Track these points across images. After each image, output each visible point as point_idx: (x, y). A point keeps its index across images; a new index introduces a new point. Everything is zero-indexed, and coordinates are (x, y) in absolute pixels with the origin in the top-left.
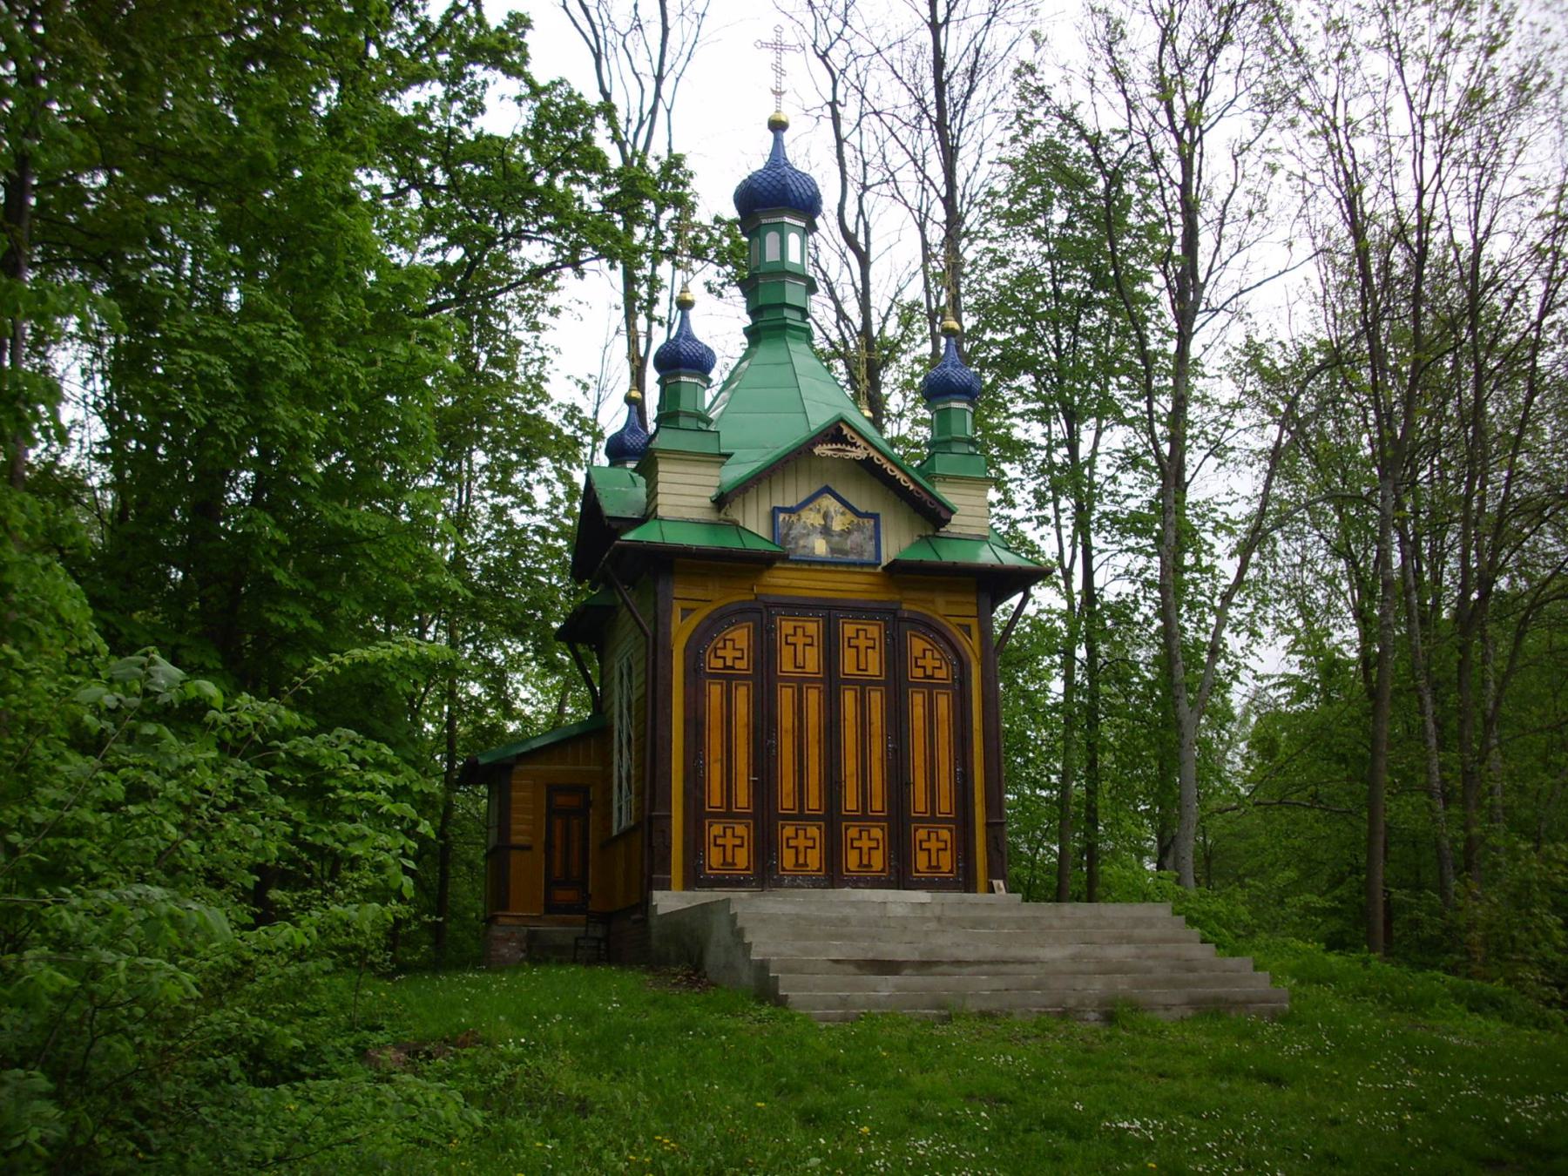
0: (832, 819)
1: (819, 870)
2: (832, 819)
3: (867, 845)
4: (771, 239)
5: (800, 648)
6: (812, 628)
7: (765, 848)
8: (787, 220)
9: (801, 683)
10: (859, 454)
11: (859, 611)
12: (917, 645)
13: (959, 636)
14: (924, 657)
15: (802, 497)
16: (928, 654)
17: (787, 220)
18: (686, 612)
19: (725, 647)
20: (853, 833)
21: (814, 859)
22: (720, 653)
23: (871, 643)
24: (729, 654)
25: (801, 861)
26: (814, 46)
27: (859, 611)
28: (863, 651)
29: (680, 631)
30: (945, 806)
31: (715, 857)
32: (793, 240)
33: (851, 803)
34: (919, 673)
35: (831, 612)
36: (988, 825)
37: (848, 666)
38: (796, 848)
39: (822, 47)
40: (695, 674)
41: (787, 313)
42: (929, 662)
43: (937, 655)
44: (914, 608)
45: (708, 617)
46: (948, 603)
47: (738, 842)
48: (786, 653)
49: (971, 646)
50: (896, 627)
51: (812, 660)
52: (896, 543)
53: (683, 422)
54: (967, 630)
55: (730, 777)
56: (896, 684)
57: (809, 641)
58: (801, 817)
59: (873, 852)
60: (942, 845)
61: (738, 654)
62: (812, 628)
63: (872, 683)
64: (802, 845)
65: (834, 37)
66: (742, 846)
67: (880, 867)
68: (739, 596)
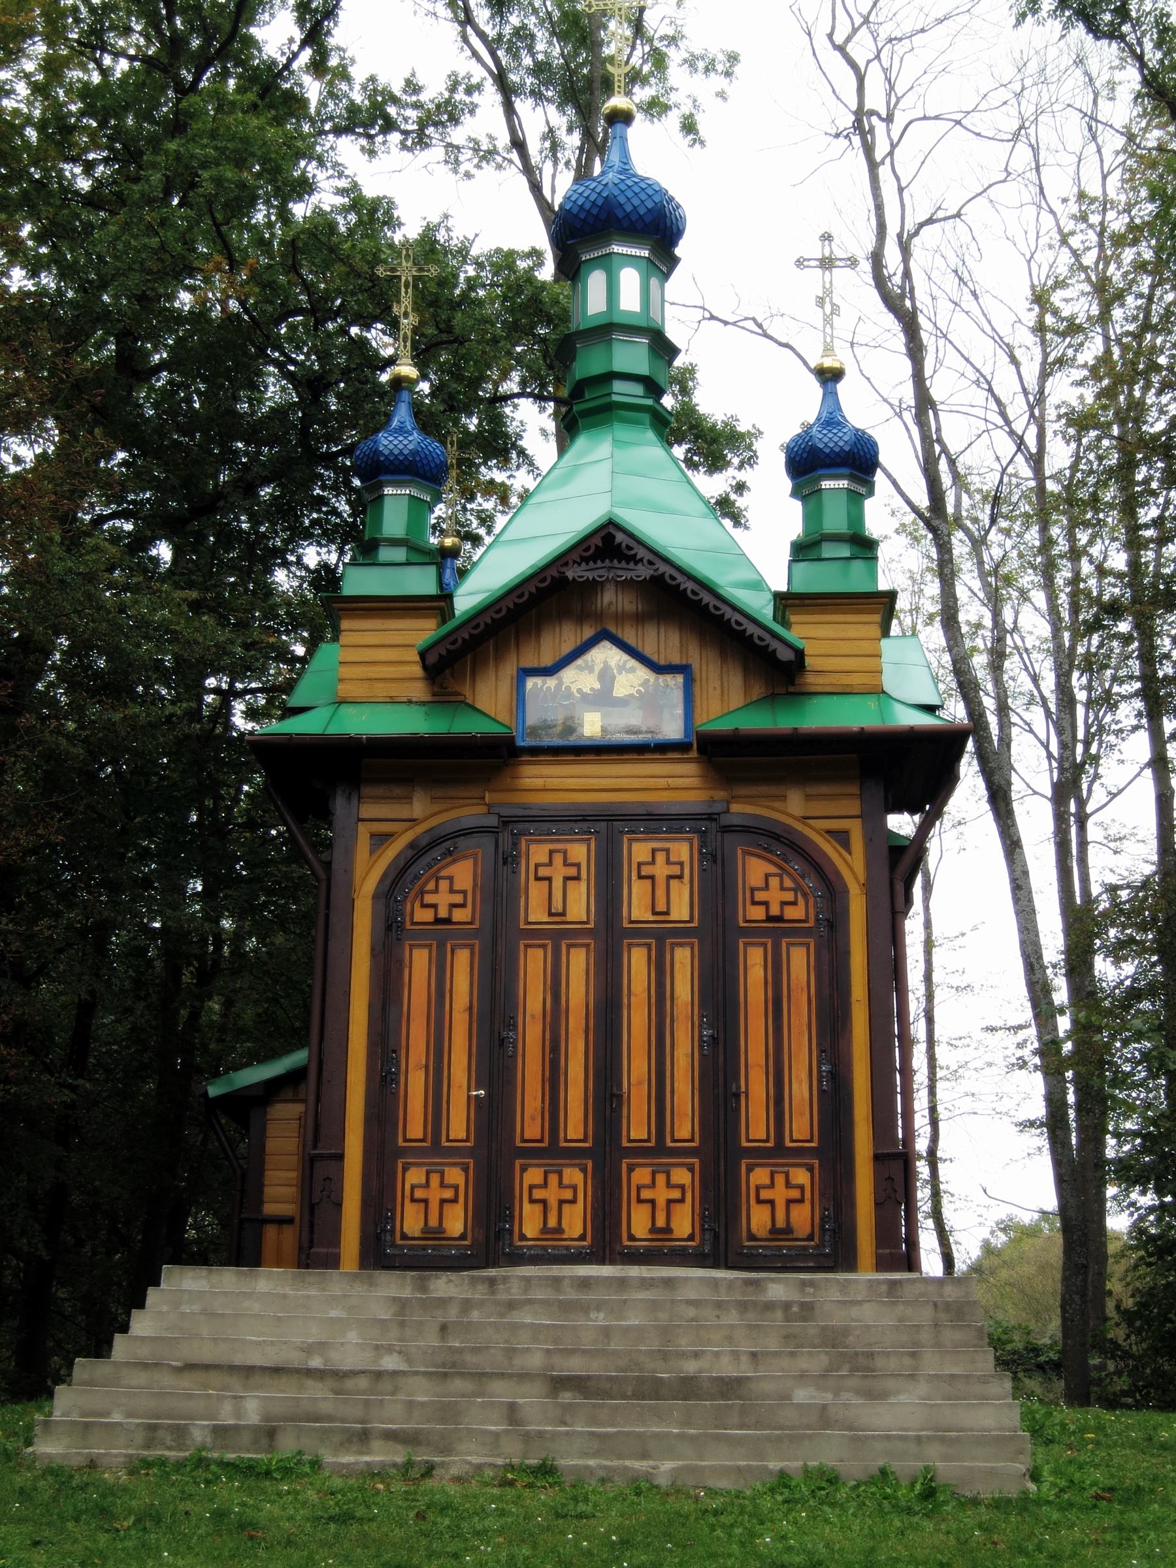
0: (606, 1154)
1: (583, 1237)
2: (606, 1154)
3: (663, 1199)
4: (596, 281)
5: (558, 883)
6: (579, 852)
7: (720, 1201)
8: (616, 249)
9: (558, 936)
10: (643, 572)
11: (655, 821)
12: (755, 870)
13: (829, 848)
14: (767, 887)
15: (567, 648)
16: (774, 882)
17: (616, 249)
18: (380, 840)
19: (436, 891)
20: (415, 1176)
21: (575, 1222)
22: (429, 899)
23: (676, 870)
24: (443, 899)
25: (552, 1223)
26: (830, 36)
27: (655, 821)
28: (663, 882)
29: (367, 873)
30: (801, 1126)
31: (411, 1222)
32: (630, 280)
33: (637, 1128)
34: (757, 913)
35: (609, 826)
36: (877, 1158)
37: (637, 906)
38: (652, 1202)
39: (839, 39)
40: (392, 932)
41: (618, 386)
42: (775, 896)
43: (788, 883)
44: (749, 809)
45: (412, 845)
46: (808, 797)
47: (448, 1194)
48: (536, 892)
49: (853, 867)
50: (717, 840)
51: (579, 904)
52: (731, 707)
53: (385, 554)
54: (842, 838)
55: (443, 1093)
56: (718, 933)
57: (572, 871)
58: (553, 1151)
59: (566, 1208)
60: (795, 1194)
61: (458, 899)
62: (579, 852)
63: (676, 933)
64: (552, 1201)
65: (858, 21)
66: (455, 1201)
67: (577, 1231)
68: (468, 812)
